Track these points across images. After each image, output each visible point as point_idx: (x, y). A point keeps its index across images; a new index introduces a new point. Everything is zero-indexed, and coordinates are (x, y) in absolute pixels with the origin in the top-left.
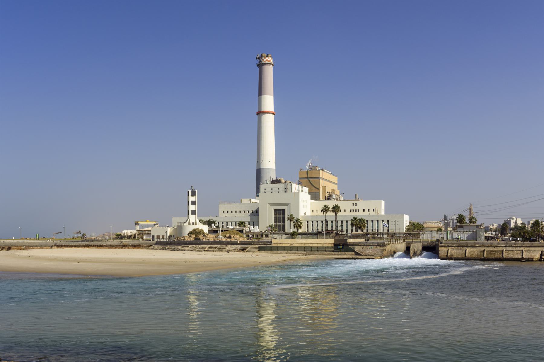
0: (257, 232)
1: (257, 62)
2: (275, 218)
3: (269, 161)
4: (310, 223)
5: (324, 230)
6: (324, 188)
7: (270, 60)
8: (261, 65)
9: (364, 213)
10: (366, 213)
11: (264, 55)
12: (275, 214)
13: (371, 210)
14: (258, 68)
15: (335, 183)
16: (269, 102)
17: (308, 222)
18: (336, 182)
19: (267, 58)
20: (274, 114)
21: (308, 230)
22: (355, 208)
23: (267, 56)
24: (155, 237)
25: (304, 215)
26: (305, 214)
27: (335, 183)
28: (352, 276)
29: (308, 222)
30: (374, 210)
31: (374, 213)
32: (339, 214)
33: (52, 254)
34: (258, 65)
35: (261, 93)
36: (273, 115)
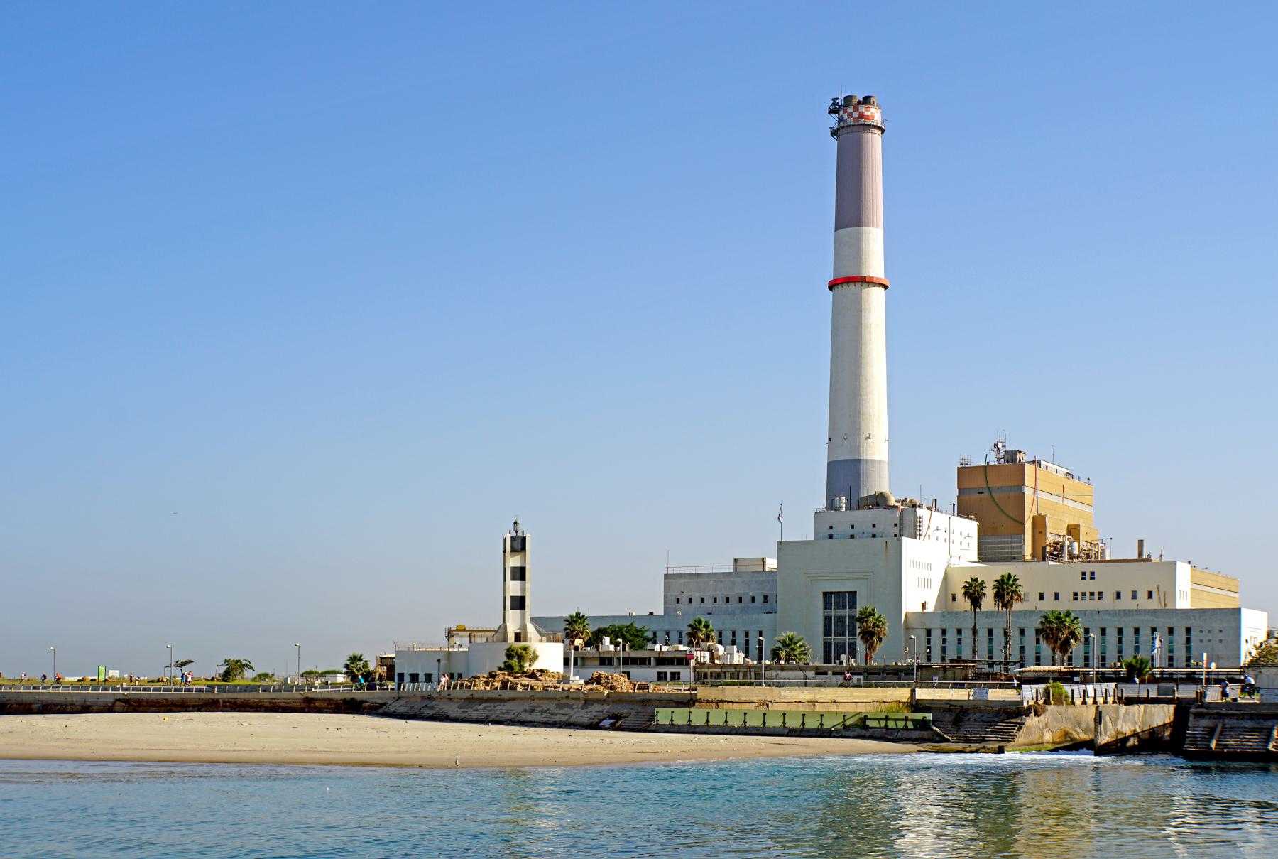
0: (736, 666)
1: (832, 121)
2: (827, 619)
4: (936, 637)
5: (936, 660)
6: (1039, 522)
10: (1126, 603)
12: (827, 605)
13: (1142, 595)
14: (834, 142)
17: (929, 632)
21: (929, 659)
22: (1088, 586)
24: (407, 678)
25: (920, 610)
26: (924, 605)
29: (929, 632)
30: (1150, 595)
31: (1153, 604)
32: (1017, 606)
33: (66, 722)
34: (834, 133)
36: (882, 289)
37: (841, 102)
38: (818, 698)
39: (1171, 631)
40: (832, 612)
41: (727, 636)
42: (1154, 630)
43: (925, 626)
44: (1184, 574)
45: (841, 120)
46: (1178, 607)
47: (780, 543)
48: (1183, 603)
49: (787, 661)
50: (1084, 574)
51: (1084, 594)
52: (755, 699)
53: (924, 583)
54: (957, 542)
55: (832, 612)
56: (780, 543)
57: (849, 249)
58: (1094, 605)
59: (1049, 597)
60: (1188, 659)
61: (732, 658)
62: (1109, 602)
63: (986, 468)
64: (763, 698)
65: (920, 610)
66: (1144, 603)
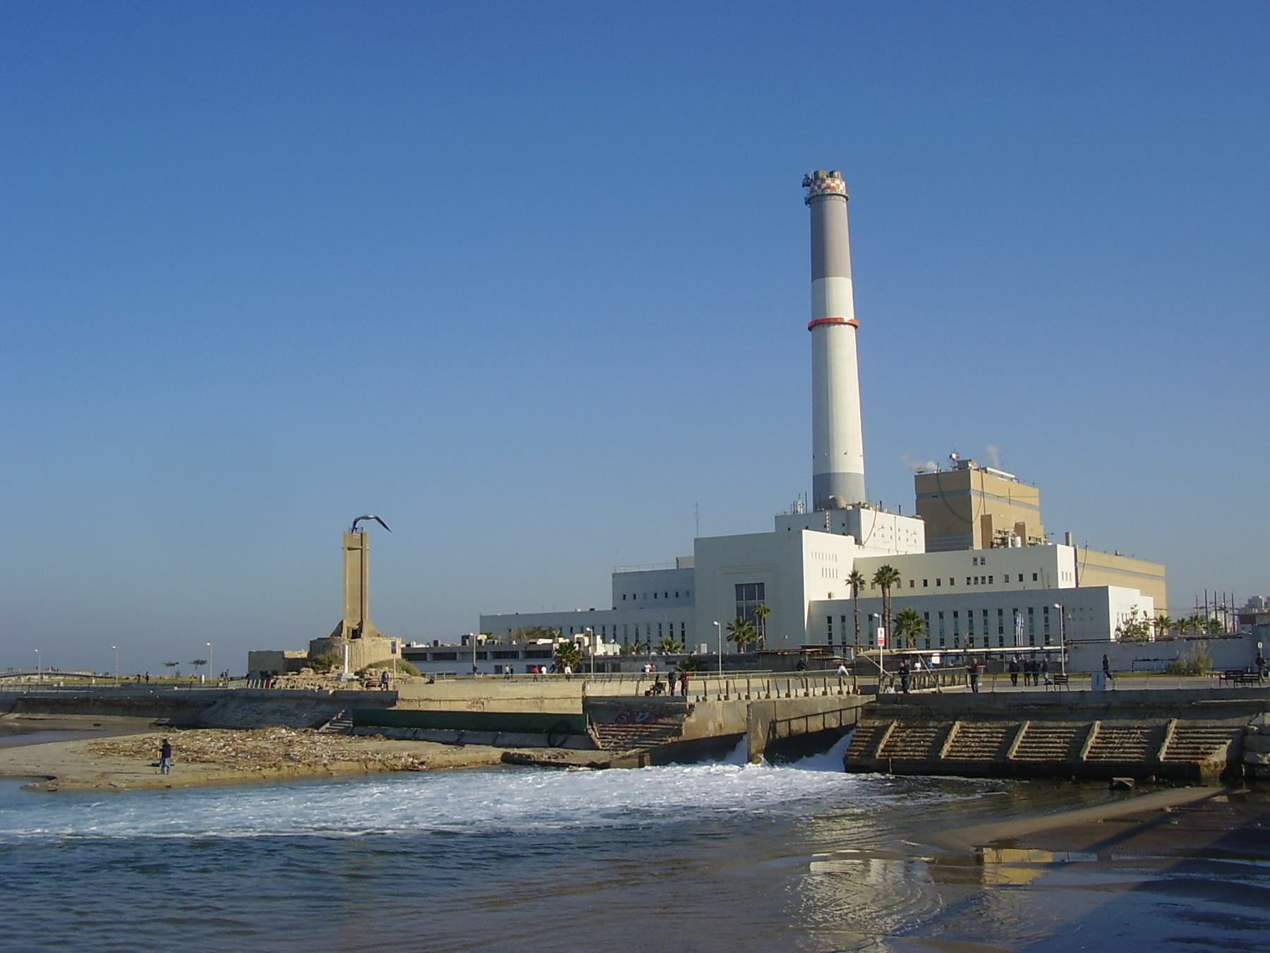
1: (806, 192)
3: (851, 457)
6: (986, 521)
7: (839, 185)
8: (817, 200)
9: (1008, 588)
11: (823, 174)
12: (739, 598)
13: (1028, 578)
14: (808, 209)
15: (1030, 506)
16: (842, 295)
18: (1036, 502)
19: (829, 181)
20: (856, 327)
22: (980, 571)
23: (831, 175)
26: (830, 596)
27: (1030, 506)
28: (46, 873)
31: (1036, 586)
34: (808, 202)
35: (820, 268)
37: (811, 176)
38: (547, 694)
39: (1031, 611)
40: (744, 603)
41: (609, 631)
42: (1015, 610)
43: (831, 612)
44: (1065, 556)
45: (812, 191)
46: (693, 554)
47: (696, 540)
48: (1066, 582)
49: (637, 652)
50: (975, 560)
51: (983, 578)
52: (466, 697)
53: (829, 573)
54: (903, 539)
55: (744, 603)
56: (696, 540)
57: (819, 297)
58: (987, 588)
59: (945, 582)
60: (1047, 637)
61: (595, 650)
62: (998, 586)
63: (938, 476)
64: (478, 696)
65: (826, 598)
66: (1029, 584)
